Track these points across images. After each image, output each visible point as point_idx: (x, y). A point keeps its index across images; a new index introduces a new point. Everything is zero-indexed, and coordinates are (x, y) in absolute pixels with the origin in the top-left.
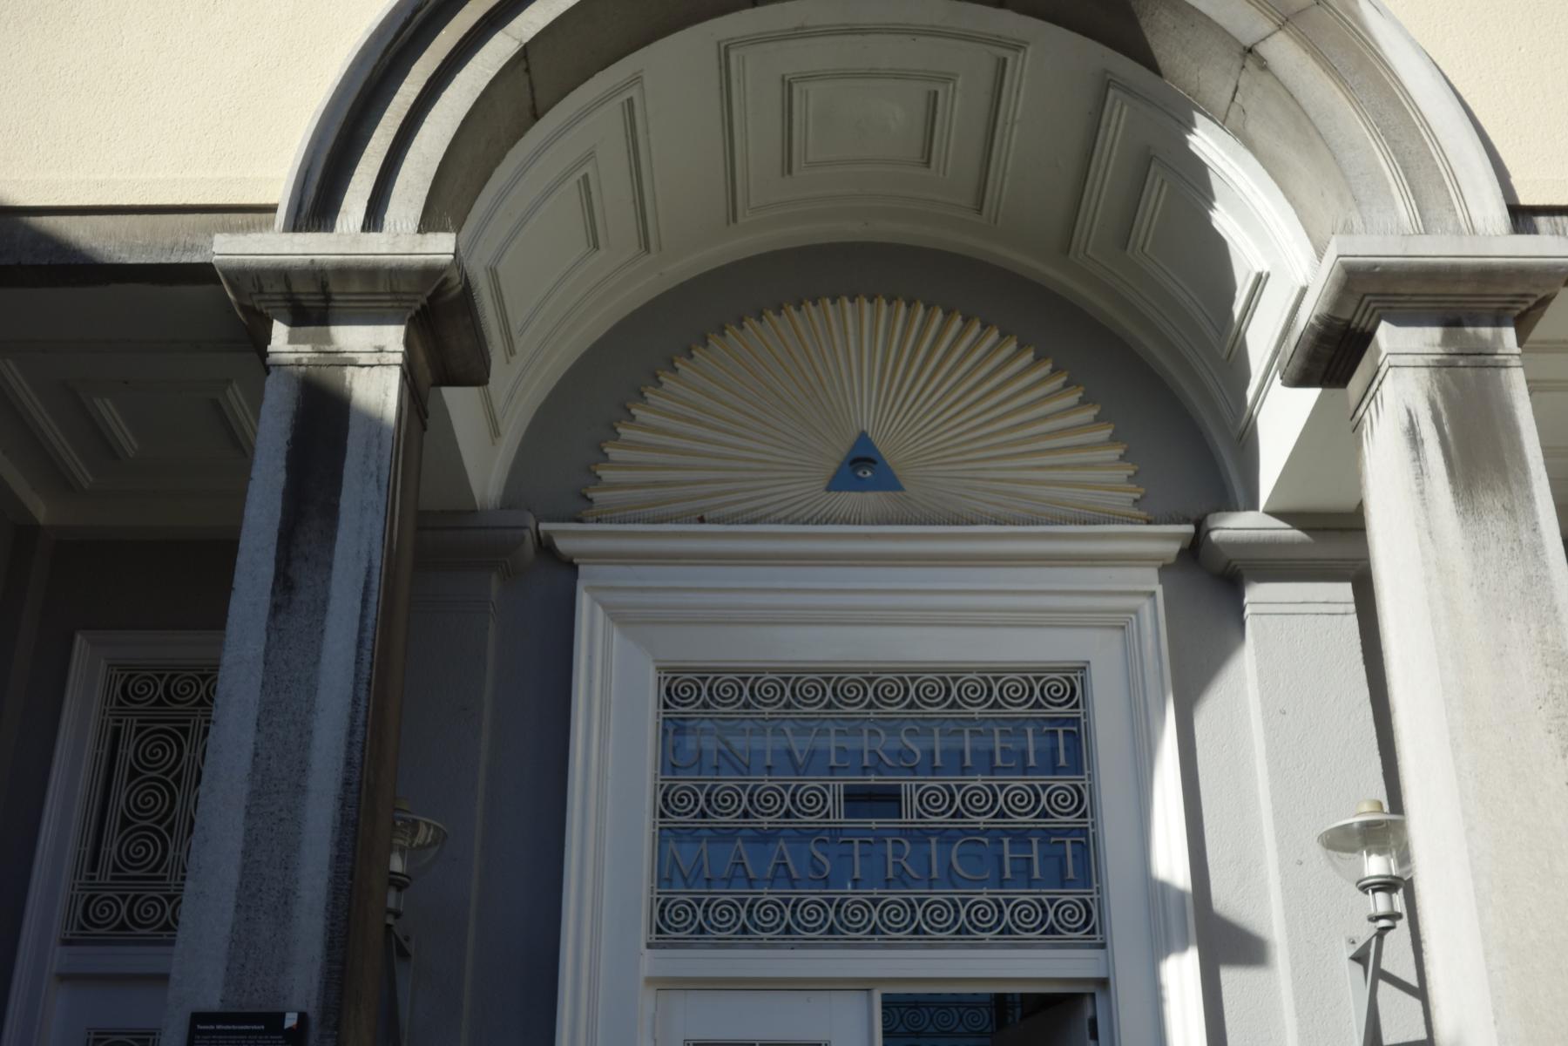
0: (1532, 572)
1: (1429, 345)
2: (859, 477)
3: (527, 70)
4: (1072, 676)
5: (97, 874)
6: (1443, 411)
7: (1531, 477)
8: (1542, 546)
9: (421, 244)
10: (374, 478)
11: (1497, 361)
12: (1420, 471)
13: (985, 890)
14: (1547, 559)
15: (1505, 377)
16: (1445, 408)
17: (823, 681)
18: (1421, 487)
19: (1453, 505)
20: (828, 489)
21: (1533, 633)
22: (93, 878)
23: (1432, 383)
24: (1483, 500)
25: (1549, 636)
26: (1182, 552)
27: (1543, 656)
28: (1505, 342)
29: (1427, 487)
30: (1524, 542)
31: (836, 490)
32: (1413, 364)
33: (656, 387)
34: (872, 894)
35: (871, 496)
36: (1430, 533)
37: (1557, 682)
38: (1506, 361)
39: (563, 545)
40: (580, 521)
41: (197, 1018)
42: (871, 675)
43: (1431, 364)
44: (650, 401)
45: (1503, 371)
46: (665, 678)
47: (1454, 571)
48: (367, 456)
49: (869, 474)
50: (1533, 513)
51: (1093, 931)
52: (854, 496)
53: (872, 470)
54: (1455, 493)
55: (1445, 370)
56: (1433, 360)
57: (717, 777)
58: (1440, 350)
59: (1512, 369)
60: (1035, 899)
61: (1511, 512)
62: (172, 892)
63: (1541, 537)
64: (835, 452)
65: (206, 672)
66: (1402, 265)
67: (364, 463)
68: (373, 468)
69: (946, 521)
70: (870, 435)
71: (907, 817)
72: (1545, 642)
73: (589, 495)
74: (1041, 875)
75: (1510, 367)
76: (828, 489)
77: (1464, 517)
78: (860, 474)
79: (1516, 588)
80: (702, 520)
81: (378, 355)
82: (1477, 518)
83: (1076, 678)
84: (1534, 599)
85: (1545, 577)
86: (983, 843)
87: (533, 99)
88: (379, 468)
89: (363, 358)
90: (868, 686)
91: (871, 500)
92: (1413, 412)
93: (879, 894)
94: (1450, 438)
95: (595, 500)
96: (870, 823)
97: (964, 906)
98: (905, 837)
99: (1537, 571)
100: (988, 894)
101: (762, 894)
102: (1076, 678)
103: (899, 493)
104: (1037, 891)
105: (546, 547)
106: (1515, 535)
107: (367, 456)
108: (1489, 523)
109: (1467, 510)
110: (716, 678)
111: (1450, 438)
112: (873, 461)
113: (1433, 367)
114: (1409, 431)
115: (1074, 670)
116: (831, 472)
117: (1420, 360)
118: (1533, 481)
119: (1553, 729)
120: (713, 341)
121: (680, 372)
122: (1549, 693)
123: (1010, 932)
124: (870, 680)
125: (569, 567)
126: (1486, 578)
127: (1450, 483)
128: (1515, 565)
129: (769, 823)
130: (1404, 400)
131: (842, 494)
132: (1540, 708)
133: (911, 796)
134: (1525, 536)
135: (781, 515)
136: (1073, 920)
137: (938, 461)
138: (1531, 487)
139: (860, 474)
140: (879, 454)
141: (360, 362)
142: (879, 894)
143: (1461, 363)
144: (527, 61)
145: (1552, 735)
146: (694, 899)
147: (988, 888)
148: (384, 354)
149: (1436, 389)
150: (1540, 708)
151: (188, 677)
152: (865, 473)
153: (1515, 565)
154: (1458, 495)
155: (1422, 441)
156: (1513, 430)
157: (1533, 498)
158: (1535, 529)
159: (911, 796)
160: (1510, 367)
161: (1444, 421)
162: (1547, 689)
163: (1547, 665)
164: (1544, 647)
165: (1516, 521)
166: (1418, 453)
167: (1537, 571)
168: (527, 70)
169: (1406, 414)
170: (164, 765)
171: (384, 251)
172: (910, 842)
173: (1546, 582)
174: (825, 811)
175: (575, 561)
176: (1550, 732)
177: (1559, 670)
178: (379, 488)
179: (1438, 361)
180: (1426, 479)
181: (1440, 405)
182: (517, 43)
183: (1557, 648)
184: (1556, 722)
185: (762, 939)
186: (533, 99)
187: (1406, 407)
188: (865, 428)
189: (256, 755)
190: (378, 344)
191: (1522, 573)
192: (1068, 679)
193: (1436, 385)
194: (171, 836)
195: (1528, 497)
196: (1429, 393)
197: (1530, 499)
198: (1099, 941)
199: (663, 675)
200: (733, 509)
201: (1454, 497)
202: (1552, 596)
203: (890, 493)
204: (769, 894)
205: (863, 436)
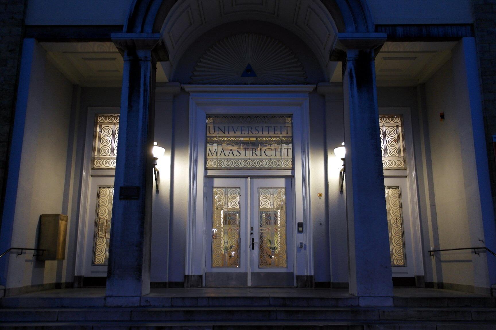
20: (241, 76)
26: (313, 90)
39: (187, 90)
41: (121, 187)
49: (250, 73)
76: (241, 76)
78: (248, 73)
125: (188, 93)
189: (127, 139)
199: (207, 116)
205: (249, 64)
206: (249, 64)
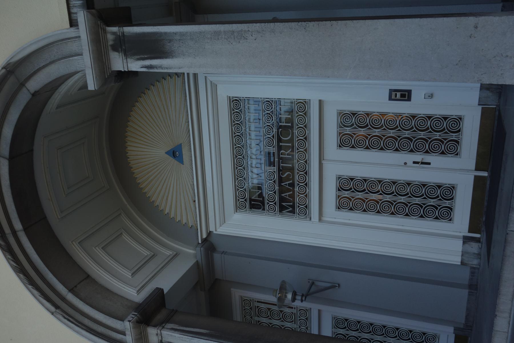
0: (189, 38)
1: (120, 57)
2: (179, 155)
3: (76, 286)
4: (232, 100)
5: (294, 307)
6: (140, 56)
7: (158, 32)
8: (180, 33)
9: (128, 329)
10: (191, 340)
11: (122, 35)
12: (160, 68)
13: (294, 131)
14: (184, 31)
15: (127, 34)
16: (139, 56)
17: (237, 169)
18: (165, 68)
19: (170, 59)
20: (183, 164)
21: (209, 41)
22: (295, 308)
23: (132, 58)
24: (167, 49)
25: (209, 36)
27: (215, 39)
28: (115, 31)
29: (166, 66)
30: (180, 38)
31: (183, 162)
32: (126, 63)
33: (159, 207)
34: (296, 162)
35: (184, 153)
36: (180, 68)
37: (223, 36)
38: (121, 33)
39: (204, 236)
40: (197, 229)
42: (235, 156)
43: (125, 58)
44: (163, 208)
45: (125, 34)
46: (239, 210)
47: (191, 63)
48: (185, 341)
49: (177, 153)
50: (170, 33)
51: (306, 102)
52: (184, 157)
53: (176, 152)
54: (166, 58)
55: (127, 53)
56: (124, 57)
57: (263, 155)
58: (121, 54)
59: (124, 31)
60: (297, 142)
61: (170, 41)
62: (298, 327)
63: (177, 32)
64: (171, 159)
65: (244, 316)
66: (95, 70)
67: (187, 341)
68: (188, 340)
69: (187, 119)
70: (166, 151)
71: (275, 170)
72: (211, 38)
73: (190, 226)
74: (290, 123)
75: (123, 31)
77: (173, 56)
78: (178, 155)
79: (194, 44)
80: (195, 201)
81: (158, 335)
82: (173, 52)
83: (232, 99)
84: (198, 39)
85: (190, 34)
86: (281, 130)
87: (83, 280)
88: (188, 339)
89: (160, 338)
90: (239, 168)
91: (185, 152)
92: (142, 66)
93: (296, 160)
94: (149, 56)
95: (192, 225)
96: (276, 160)
97: (299, 125)
98: (280, 152)
99: (189, 36)
100: (295, 130)
101: (296, 190)
102: (232, 99)
103: (182, 145)
104: (294, 117)
105: (204, 241)
106: (178, 41)
107: (185, 341)
108: (175, 49)
109: (171, 55)
110: (238, 186)
111: (149, 56)
112: (174, 151)
113: (126, 57)
114: (148, 69)
115: (230, 100)
116: (178, 163)
117: (125, 61)
118: (160, 31)
119: (238, 41)
120: (145, 325)
121: (154, 200)
122: (227, 40)
123: (306, 161)
124: (236, 157)
126: (192, 53)
127: (163, 59)
128: (187, 43)
129: (277, 187)
130: (138, 68)
131: (184, 160)
132: (232, 44)
133: (269, 149)
134: (178, 38)
135: (191, 177)
136: (302, 107)
137: (171, 131)
138: (162, 32)
139: (178, 155)
140: (172, 149)
141: (161, 339)
142: (296, 160)
143: (124, 48)
144: (73, 288)
145: (240, 42)
146: (297, 174)
147: (294, 130)
148: (158, 333)
149: (133, 57)
150: (232, 44)
151: (245, 320)
152: (177, 154)
153: (187, 43)
154: (167, 57)
155: (151, 65)
156: (144, 34)
157: (165, 32)
158: (175, 34)
159: (269, 149)
160: (123, 31)
161: (144, 57)
162: (226, 40)
163: (218, 39)
164: (213, 38)
165: (173, 40)
166: (155, 67)
167: (189, 36)
168: (76, 286)
169: (143, 68)
170: (267, 311)
171: (131, 337)
172: (281, 150)
173: (192, 34)
174: (273, 146)
175: (209, 232)
176: (239, 42)
177: (219, 35)
178: (193, 339)
179: (124, 55)
180: (162, 66)
181: (138, 57)
182: (69, 293)
183: (213, 34)
184: (236, 39)
185: (308, 192)
186: (83, 280)
187: (140, 68)
188: (165, 152)
190: (156, 335)
191: (190, 41)
192: (233, 101)
193: (132, 57)
194: (285, 326)
195: (165, 34)
196: (134, 60)
197: (166, 33)
198: (308, 101)
199: (238, 210)
200: (191, 190)
201: (167, 58)
202: (196, 32)
203: (183, 147)
204: (296, 189)
206: (166, 153)
